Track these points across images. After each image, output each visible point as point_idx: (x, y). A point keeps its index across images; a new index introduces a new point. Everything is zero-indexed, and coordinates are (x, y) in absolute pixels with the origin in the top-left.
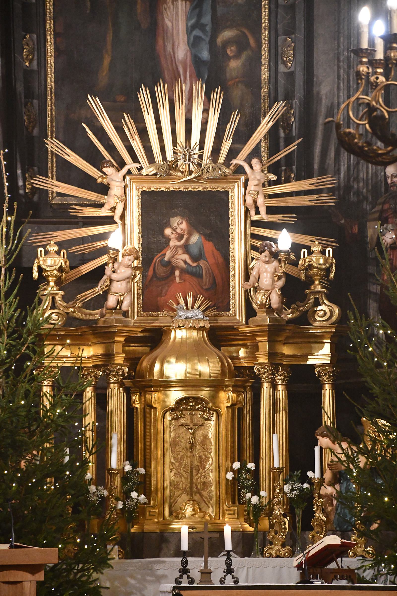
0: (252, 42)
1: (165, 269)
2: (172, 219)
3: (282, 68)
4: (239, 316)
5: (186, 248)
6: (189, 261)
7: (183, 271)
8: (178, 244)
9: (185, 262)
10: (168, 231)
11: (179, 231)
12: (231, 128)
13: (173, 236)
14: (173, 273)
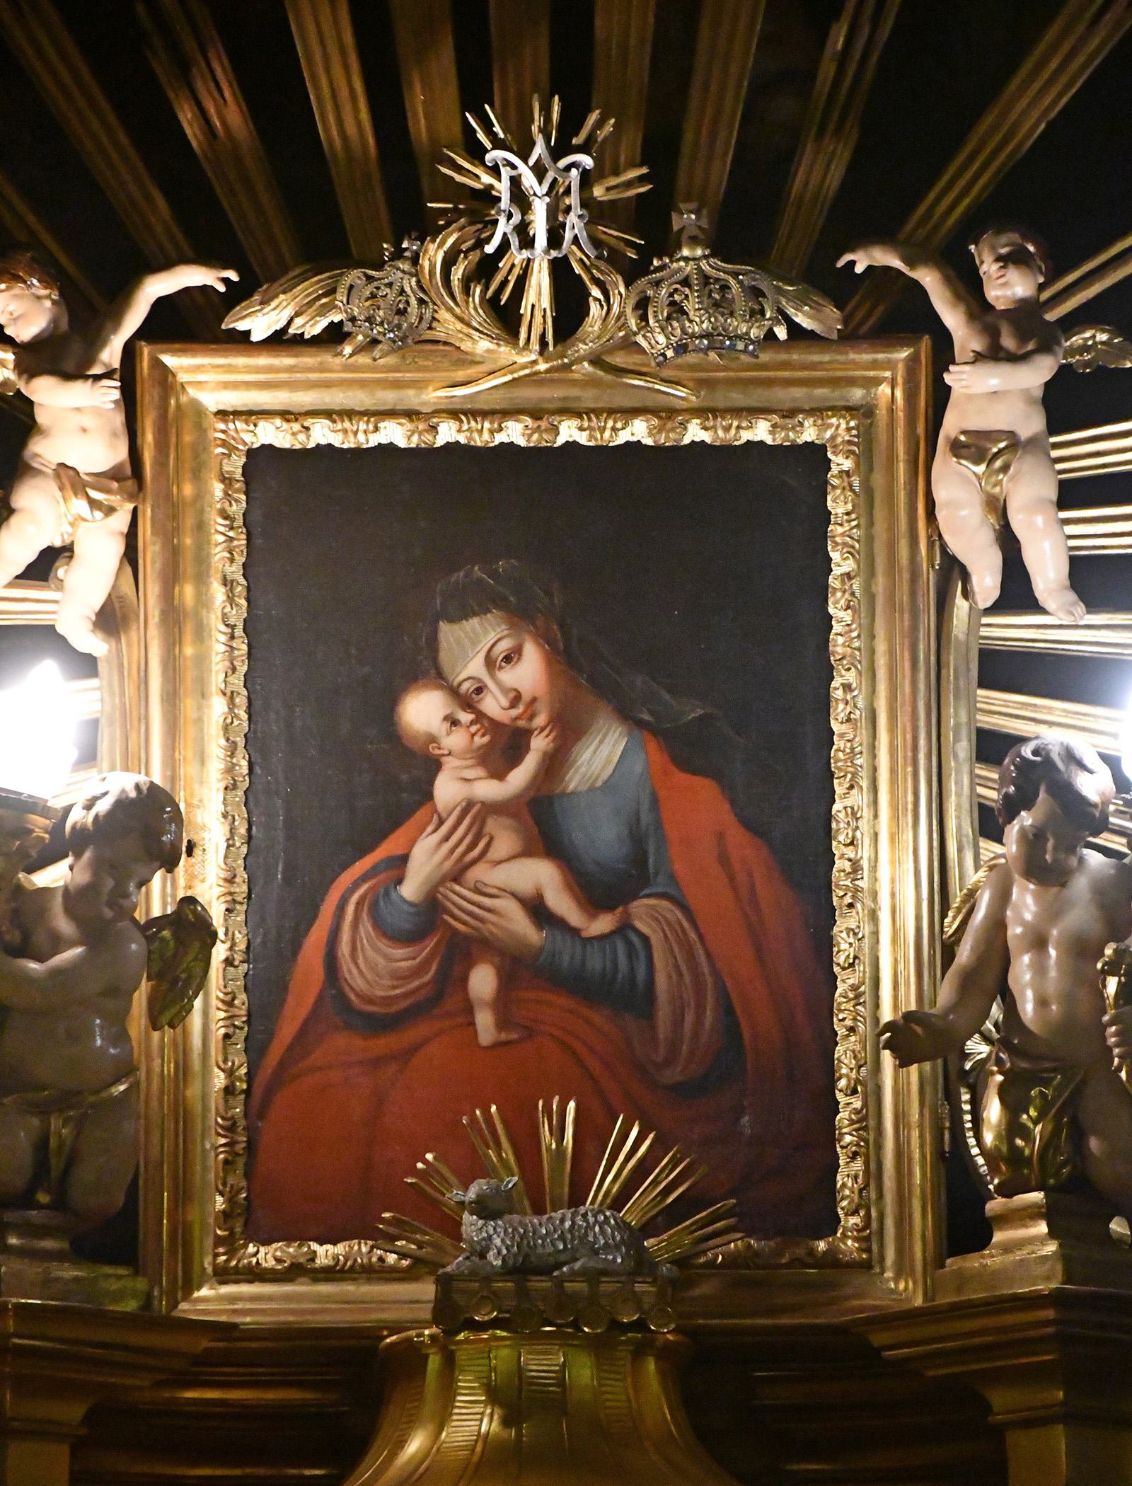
1: (402, 957)
2: (448, 633)
6: (561, 903)
8: (489, 790)
9: (536, 908)
11: (494, 705)
13: (455, 741)
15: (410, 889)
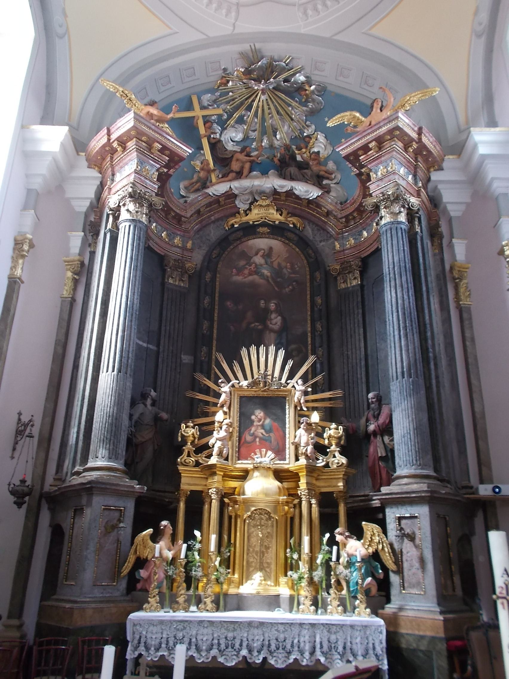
0: (304, 350)
1: (251, 437)
2: (255, 411)
3: (315, 283)
4: (158, 164)
5: (263, 426)
6: (264, 433)
7: (261, 439)
8: (259, 424)
9: (262, 434)
10: (253, 417)
11: (259, 417)
12: (287, 368)
13: (256, 420)
14: (255, 440)
15: (252, 432)
